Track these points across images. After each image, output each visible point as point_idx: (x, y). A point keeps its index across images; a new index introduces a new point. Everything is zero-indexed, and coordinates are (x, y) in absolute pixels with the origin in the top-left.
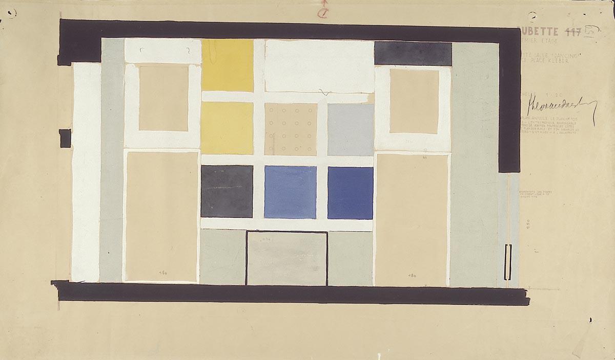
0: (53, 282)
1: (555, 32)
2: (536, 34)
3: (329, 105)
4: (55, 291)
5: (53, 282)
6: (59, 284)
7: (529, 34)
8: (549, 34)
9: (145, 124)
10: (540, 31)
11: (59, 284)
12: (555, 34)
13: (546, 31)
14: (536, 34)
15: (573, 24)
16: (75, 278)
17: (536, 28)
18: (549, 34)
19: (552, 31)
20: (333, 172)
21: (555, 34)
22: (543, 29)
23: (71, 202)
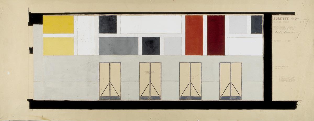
0: (28, 100)
1: (288, 19)
2: (281, 20)
3: (100, 54)
4: (28, 103)
5: (28, 100)
6: (31, 101)
7: (278, 20)
8: (286, 20)
9: (262, 16)
10: (282, 19)
11: (31, 101)
12: (288, 20)
13: (287, 19)
14: (281, 20)
15: (129, 86)
16: (35, 99)
17: (281, 18)
18: (286, 20)
19: (287, 19)
20: (201, 53)
21: (288, 20)
22: (283, 18)
23: (102, 55)
